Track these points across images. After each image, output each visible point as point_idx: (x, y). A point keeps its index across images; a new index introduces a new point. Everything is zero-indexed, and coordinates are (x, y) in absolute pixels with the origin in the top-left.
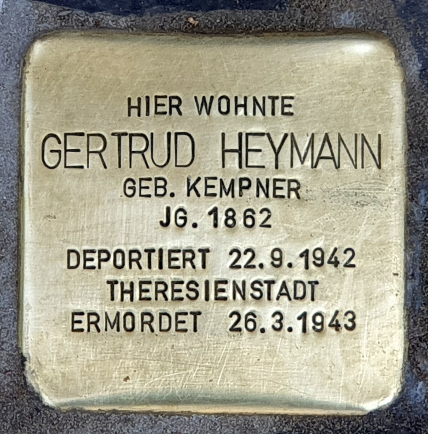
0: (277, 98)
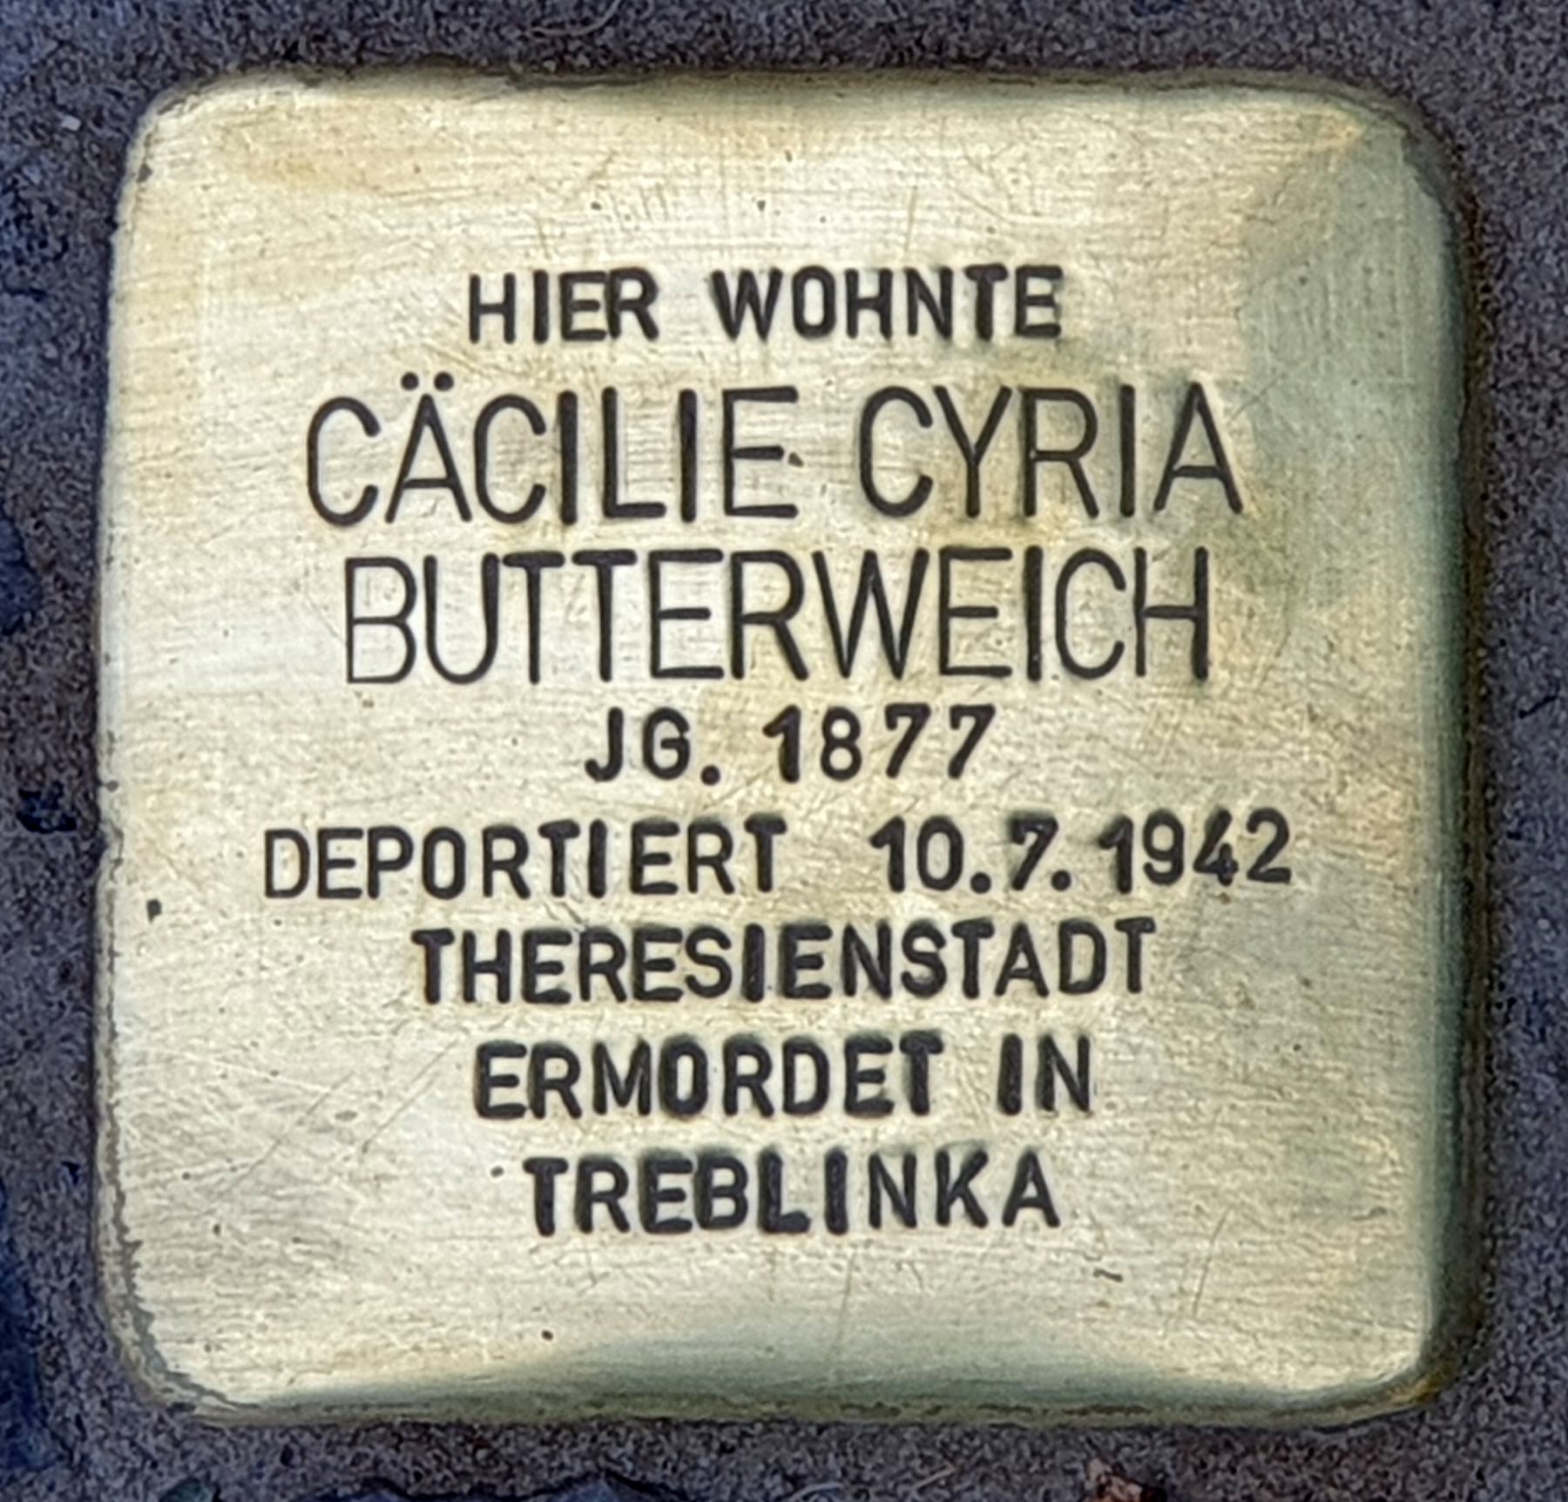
0: (999, 272)
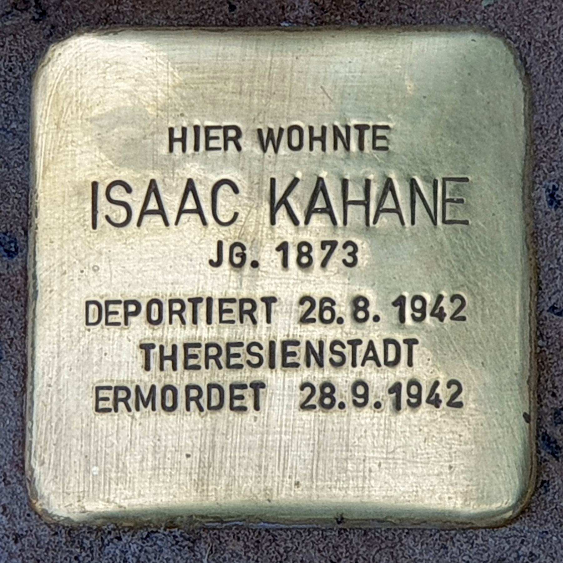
0: (367, 127)
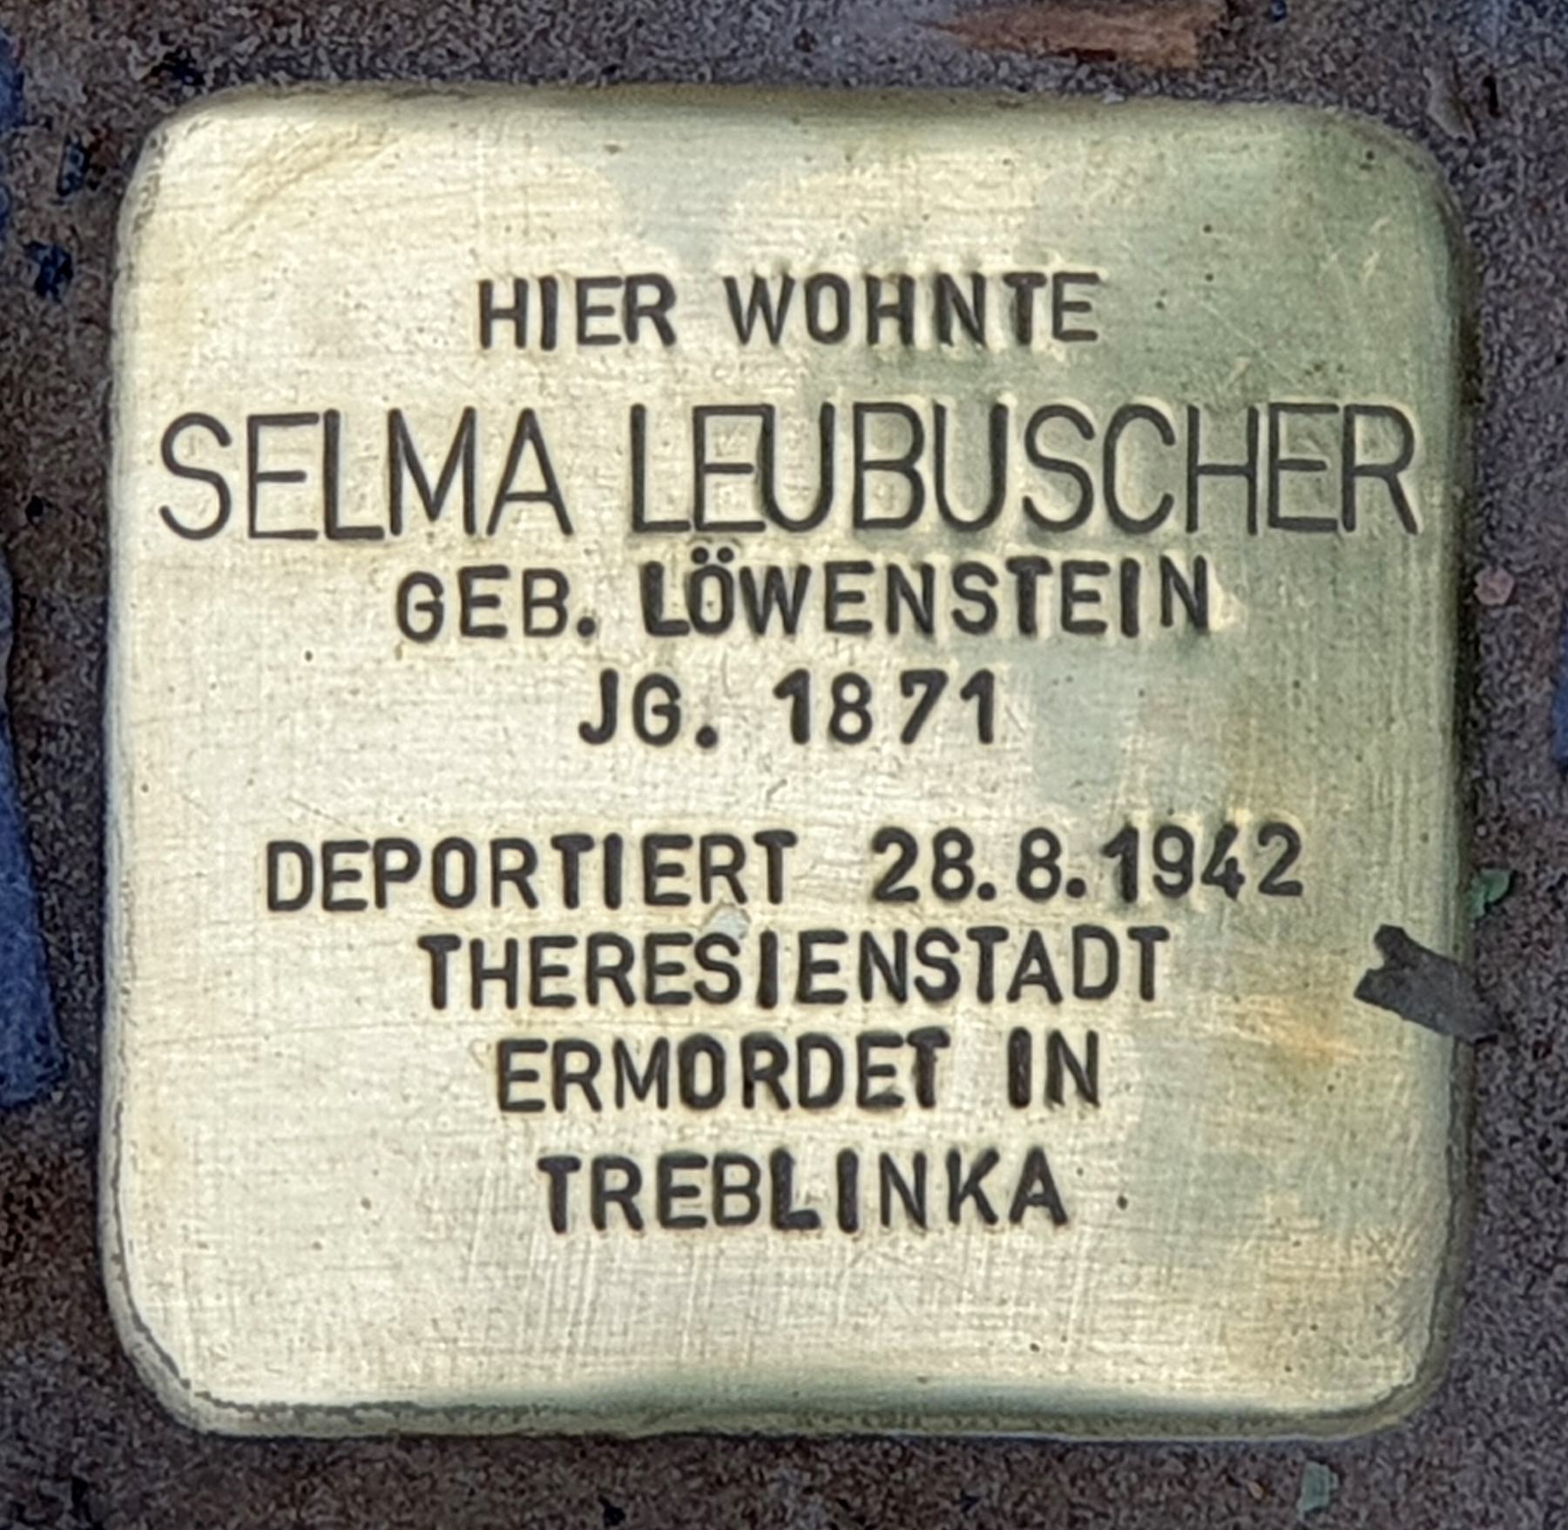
0: (1037, 279)
